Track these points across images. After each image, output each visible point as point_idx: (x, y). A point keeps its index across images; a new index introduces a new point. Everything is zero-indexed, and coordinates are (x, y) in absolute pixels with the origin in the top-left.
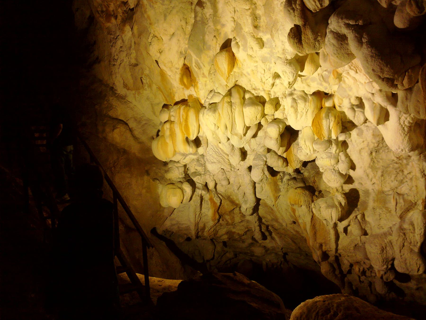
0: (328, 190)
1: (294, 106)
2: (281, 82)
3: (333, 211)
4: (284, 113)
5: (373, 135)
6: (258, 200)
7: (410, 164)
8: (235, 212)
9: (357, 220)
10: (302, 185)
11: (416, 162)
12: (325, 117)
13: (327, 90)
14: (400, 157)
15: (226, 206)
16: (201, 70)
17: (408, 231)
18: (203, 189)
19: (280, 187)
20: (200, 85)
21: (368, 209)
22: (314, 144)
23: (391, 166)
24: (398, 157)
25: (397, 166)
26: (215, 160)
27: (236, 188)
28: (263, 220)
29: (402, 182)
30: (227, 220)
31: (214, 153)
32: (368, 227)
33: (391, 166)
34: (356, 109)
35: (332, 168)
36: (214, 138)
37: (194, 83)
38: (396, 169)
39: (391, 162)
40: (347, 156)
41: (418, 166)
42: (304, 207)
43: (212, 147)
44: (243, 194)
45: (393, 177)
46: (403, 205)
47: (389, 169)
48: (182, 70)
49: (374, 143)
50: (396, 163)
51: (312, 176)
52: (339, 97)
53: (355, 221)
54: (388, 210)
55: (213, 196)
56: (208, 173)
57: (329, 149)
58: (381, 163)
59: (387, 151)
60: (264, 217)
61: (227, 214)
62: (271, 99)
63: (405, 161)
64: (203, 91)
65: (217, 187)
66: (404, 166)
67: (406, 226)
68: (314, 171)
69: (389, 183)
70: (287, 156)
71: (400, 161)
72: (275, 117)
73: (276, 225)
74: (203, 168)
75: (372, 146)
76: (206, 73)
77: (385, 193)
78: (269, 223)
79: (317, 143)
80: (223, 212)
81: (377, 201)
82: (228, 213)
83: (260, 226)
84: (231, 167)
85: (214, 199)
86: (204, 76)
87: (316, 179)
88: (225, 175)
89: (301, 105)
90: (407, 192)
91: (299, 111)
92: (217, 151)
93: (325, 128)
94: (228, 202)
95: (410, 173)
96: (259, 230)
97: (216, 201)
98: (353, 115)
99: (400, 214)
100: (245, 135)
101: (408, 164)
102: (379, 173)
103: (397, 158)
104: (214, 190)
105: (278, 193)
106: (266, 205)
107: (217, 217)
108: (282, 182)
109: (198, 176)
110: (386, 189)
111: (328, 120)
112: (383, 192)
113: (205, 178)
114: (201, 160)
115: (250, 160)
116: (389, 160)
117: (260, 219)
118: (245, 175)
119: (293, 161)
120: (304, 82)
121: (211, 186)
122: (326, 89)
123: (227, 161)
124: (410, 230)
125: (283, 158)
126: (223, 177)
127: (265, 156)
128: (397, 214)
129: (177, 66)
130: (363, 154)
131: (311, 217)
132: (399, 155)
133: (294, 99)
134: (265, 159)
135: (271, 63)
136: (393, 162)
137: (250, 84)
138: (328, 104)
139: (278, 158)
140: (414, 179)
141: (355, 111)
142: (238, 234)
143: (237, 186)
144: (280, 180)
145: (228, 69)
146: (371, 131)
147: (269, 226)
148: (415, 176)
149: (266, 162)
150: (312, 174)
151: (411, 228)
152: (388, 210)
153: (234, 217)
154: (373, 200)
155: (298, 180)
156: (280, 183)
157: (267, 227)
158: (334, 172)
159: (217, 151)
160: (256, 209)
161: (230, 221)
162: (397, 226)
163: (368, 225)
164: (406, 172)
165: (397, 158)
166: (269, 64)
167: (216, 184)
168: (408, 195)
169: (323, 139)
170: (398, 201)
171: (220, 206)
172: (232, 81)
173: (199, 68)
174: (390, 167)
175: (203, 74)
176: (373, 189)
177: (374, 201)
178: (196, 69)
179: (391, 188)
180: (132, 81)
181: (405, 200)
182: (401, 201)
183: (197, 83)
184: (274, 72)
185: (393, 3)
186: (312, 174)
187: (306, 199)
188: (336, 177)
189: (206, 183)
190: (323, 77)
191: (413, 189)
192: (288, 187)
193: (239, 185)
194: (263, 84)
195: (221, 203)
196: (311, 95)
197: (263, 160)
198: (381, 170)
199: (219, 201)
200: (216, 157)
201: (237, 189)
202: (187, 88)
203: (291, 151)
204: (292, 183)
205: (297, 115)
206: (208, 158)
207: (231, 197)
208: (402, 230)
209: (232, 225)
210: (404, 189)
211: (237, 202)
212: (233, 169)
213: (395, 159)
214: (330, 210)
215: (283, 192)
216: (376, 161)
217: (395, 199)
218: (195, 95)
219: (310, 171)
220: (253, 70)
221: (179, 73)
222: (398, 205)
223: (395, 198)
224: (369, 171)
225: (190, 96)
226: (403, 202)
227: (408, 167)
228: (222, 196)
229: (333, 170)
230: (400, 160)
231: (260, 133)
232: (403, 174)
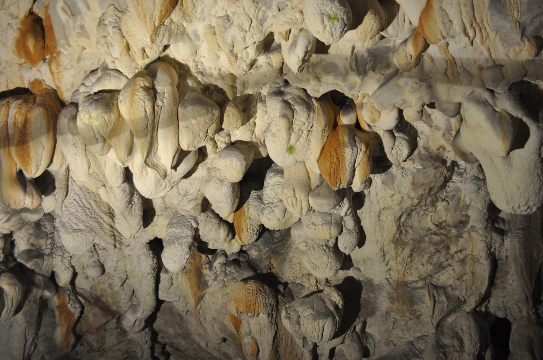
0: (298, 282)
1: (289, 116)
2: (269, 60)
3: (327, 323)
4: (253, 132)
5: (413, 184)
6: (159, 303)
7: (465, 235)
8: (107, 328)
9: (355, 334)
10: (248, 273)
11: (481, 232)
12: (350, 143)
13: (353, 92)
14: (441, 224)
15: (91, 318)
16: (79, 17)
17: (451, 349)
20: (64, 60)
21: (378, 313)
22: (313, 196)
23: (427, 239)
24: (437, 223)
25: (436, 238)
26: (81, 224)
27: (117, 283)
28: (160, 339)
29: (440, 267)
30: (89, 344)
31: (80, 209)
32: (370, 343)
33: (427, 239)
34: (396, 134)
35: (324, 244)
36: (90, 175)
37: (52, 54)
38: (436, 244)
39: (426, 233)
40: (357, 221)
41: (484, 238)
42: (263, 317)
43: (76, 197)
44: (129, 294)
45: (426, 257)
46: (446, 305)
47: (423, 245)
48: (23, 23)
49: (412, 199)
50: (435, 234)
52: (373, 107)
53: (352, 336)
54: (414, 314)
55: (67, 300)
56: (59, 253)
57: (338, 207)
58: (410, 235)
59: (422, 213)
60: (162, 331)
61: (92, 333)
62: (235, 98)
63: (454, 231)
64: (72, 72)
65: (77, 281)
66: (453, 240)
67: (446, 341)
69: (416, 269)
70: (234, 220)
71: (442, 231)
72: (233, 139)
73: (182, 343)
74: (49, 241)
75: (407, 204)
76: (91, 24)
77: (410, 286)
78: (167, 340)
79: (318, 195)
80: (84, 329)
81: (398, 300)
82: (95, 330)
83: (152, 348)
84: (115, 240)
85: (69, 305)
86: (83, 32)
87: (273, 261)
88: (96, 257)
89: (300, 115)
90: (450, 282)
91: (295, 127)
92: (87, 205)
93: (347, 163)
94: (96, 310)
95: (461, 251)
96: (150, 355)
97: (72, 310)
98: (391, 145)
99: (438, 321)
100: (175, 168)
101: (459, 236)
102: (407, 251)
103: (436, 225)
104: (69, 287)
106: (171, 310)
107: (72, 340)
108: (211, 268)
110: (410, 279)
111: (355, 149)
112: (405, 284)
113: (51, 264)
114: (44, 226)
115: (159, 228)
116: (422, 229)
117: (154, 335)
118: (143, 257)
119: (245, 230)
120: (311, 70)
121: (63, 278)
122: (352, 88)
123: (108, 227)
124: (454, 346)
125: (226, 222)
126: (92, 260)
127: (195, 220)
128: (433, 321)
129: (13, 10)
130: (383, 217)
131: (274, 333)
132: (440, 221)
133: (286, 102)
134: (195, 225)
135: (269, 7)
136: (430, 232)
137: (194, 61)
138: (346, 120)
139: (219, 224)
140: (469, 261)
141: (394, 137)
143: (120, 278)
144: (208, 266)
145: (162, 5)
146: (410, 177)
147: (166, 345)
148: (470, 256)
149: (197, 230)
150: (265, 254)
151: (456, 343)
152: (414, 314)
153: (104, 337)
154: (390, 298)
155: (242, 264)
156: (206, 272)
157: (164, 346)
158: (327, 251)
159: (87, 205)
160: (150, 320)
161: (95, 345)
162: (431, 341)
163: (370, 340)
164: (453, 249)
165: (436, 225)
166: (264, 8)
167: (75, 275)
168: (452, 288)
169: (338, 185)
170: (436, 298)
171: (79, 318)
172: (162, 41)
173: (73, 13)
174: (424, 241)
175: (82, 27)
176: (387, 279)
177: (392, 299)
178: (64, 17)
179: (419, 277)
181: (448, 297)
182: (443, 298)
183: (59, 53)
184: (270, 30)
186: (265, 254)
187: (267, 301)
189: (53, 273)
190: (357, 62)
191: (464, 278)
192: (226, 279)
193: (125, 276)
194: (233, 58)
195: (82, 312)
196: (317, 99)
197: (192, 226)
198: (410, 247)
199: (79, 310)
200: (84, 218)
201: (120, 284)
202: (32, 61)
203: (244, 211)
204: (234, 271)
205: (290, 135)
206: (65, 220)
207: (103, 299)
208: (442, 348)
209: (98, 351)
210: (445, 278)
211: (114, 308)
212: (118, 245)
213: (433, 227)
214: (321, 322)
215: (214, 286)
216: (404, 231)
217: (432, 295)
218: (49, 82)
219: (261, 247)
220: (212, 27)
221: (15, 27)
222: (436, 306)
223: (431, 293)
224: (390, 249)
225: (38, 82)
226: (446, 301)
227: (461, 240)
229: (325, 248)
230: (441, 228)
231: (201, 171)
232: (448, 253)
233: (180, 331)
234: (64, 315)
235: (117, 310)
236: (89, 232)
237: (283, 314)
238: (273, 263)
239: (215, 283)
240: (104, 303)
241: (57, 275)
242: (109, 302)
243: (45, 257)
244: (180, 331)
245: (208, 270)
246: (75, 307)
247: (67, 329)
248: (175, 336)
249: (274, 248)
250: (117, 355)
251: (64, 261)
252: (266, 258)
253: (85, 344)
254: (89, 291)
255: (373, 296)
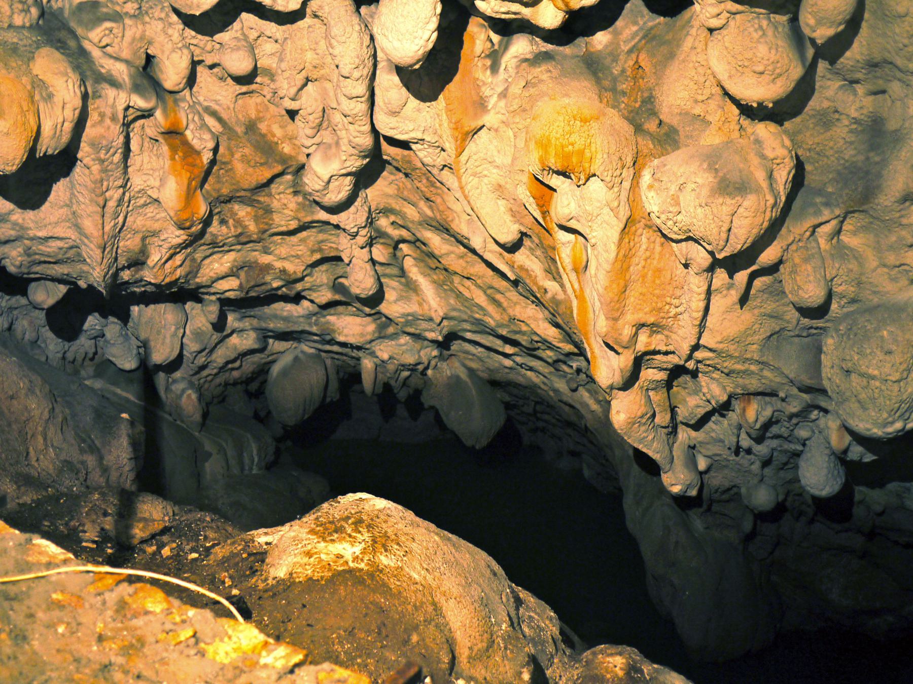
15: (239, 168)
18: (137, 88)
19: (486, 91)
30: (238, 222)
51: (626, 48)
68: (635, 28)
85: (188, 133)
97: (196, 143)
105: (476, 116)
109: (108, 24)
142: (284, 271)
144: (488, 62)
171: (213, 162)
180: (408, 263)
185: (11, 505)
188: (773, 56)
189: (149, 58)
228: (220, 120)
233: (429, 212)
234: (181, 154)
235: (293, 154)
236: (378, 613)
237: (646, 178)
238: (642, 64)
239: (502, 103)
240: (263, 136)
241: (157, 65)
242: (274, 136)
243: (128, 21)
244: (429, 212)
245: (488, 72)
246: (201, 139)
247: (189, 184)
248: (420, 224)
249: (652, 28)
250: (299, 253)
251: (170, 31)
252: (630, 51)
253: (231, 222)
254: (232, 106)
255: (877, 159)
